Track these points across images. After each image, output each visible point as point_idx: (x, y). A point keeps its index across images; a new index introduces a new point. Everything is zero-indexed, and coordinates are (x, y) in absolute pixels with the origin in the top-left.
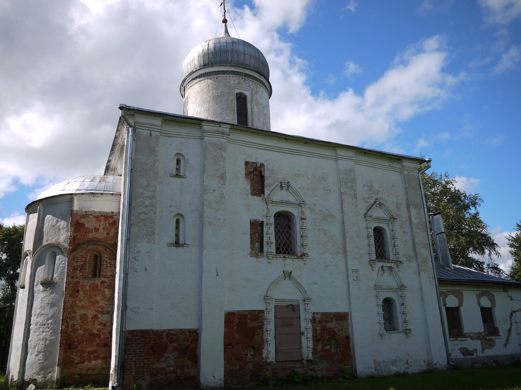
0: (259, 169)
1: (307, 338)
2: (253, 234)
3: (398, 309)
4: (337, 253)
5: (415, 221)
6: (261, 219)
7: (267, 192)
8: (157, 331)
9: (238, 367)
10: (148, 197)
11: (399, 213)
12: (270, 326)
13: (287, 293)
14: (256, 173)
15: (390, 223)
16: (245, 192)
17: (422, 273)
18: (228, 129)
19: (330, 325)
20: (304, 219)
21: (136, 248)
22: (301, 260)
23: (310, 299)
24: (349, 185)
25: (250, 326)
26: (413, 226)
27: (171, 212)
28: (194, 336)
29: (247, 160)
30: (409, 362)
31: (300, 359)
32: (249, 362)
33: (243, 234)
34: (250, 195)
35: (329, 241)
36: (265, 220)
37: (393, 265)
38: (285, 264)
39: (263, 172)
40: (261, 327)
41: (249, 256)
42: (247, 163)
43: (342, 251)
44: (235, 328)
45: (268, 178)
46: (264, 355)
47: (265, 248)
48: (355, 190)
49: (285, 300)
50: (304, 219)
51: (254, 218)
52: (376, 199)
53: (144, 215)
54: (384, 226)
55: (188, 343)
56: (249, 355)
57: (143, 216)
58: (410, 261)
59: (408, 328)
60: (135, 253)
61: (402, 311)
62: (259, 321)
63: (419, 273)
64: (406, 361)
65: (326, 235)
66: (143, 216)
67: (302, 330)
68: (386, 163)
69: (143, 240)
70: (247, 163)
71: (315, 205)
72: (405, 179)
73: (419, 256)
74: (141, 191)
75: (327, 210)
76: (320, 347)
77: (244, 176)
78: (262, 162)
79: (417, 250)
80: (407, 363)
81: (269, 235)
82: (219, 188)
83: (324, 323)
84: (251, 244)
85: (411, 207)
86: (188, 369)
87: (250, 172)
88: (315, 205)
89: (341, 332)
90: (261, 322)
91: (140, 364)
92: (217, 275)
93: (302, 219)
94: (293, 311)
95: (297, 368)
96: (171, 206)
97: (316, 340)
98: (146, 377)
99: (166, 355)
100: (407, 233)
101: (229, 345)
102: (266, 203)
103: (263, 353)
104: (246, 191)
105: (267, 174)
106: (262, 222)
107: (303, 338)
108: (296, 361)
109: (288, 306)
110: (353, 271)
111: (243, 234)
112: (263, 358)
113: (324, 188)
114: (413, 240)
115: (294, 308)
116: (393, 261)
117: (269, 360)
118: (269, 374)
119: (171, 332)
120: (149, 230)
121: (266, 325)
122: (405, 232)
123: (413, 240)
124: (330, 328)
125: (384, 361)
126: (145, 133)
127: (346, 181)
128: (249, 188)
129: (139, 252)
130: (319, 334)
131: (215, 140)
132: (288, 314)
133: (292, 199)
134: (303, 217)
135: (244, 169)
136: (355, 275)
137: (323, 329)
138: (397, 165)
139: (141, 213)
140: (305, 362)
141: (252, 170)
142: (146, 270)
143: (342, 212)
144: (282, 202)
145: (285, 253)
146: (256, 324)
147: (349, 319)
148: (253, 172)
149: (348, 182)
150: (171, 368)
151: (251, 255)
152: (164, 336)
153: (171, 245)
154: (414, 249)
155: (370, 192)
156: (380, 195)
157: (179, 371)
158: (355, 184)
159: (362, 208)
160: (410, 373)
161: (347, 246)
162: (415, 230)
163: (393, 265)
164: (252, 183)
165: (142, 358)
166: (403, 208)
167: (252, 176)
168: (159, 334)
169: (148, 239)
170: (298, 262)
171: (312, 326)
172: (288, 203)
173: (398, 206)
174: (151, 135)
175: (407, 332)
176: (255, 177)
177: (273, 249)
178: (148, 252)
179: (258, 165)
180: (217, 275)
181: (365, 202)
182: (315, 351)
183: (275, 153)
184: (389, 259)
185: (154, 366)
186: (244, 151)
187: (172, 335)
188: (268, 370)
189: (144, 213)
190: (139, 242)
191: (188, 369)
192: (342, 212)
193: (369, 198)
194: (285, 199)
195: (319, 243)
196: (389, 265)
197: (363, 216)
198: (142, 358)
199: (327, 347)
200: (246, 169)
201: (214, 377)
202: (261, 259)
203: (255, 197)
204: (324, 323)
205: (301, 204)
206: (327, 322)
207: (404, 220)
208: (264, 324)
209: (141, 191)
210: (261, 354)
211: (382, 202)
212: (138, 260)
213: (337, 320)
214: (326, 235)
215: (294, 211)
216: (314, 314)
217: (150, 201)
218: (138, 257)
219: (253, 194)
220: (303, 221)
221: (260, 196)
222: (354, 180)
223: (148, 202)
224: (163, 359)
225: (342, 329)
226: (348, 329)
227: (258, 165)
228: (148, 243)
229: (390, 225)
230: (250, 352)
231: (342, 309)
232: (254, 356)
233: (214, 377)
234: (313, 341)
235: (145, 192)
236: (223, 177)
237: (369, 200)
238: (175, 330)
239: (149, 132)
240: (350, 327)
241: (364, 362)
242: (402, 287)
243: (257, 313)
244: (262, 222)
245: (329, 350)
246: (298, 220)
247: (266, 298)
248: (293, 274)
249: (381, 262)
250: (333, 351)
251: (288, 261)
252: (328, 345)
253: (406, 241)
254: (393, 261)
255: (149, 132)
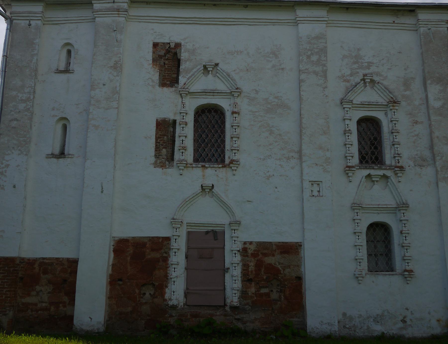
0: (173, 51)
1: (232, 276)
2: (159, 138)
3: (396, 239)
4: (288, 159)
5: (435, 104)
6: (171, 117)
7: (182, 80)
8: (29, 260)
9: (129, 309)
10: (22, 100)
11: (408, 93)
12: (178, 260)
13: (206, 214)
14: (168, 56)
15: (388, 109)
16: (151, 84)
17: (441, 184)
18: (126, 5)
19: (270, 260)
20: (238, 113)
21: (4, 162)
22: (228, 169)
23: (239, 223)
24: (314, 58)
25: (149, 257)
26: (431, 112)
27: (54, 116)
28: (72, 265)
29: (157, 41)
30: (407, 320)
31: (223, 304)
32: (146, 303)
33: (146, 138)
34: (157, 87)
35: (276, 142)
36: (178, 118)
37: (389, 173)
38: (204, 176)
39: (178, 55)
40: (166, 259)
41: (152, 166)
42: (155, 45)
43: (296, 156)
44: (129, 258)
45: (186, 61)
46: (167, 296)
47: (177, 156)
48: (324, 65)
49: (203, 225)
50: (238, 113)
51: (162, 116)
52: (365, 75)
53: (15, 122)
54: (380, 115)
55: (63, 275)
56: (147, 295)
57: (14, 124)
58: (421, 166)
59: (408, 268)
60: (3, 168)
61: (401, 242)
62: (163, 251)
63: (437, 183)
64: (401, 318)
65: (271, 133)
66: (14, 124)
67: (227, 265)
68: (389, 19)
69: (13, 151)
70: (155, 45)
71: (257, 92)
72: (421, 40)
73: (438, 158)
74: (14, 93)
75: (276, 98)
76: (253, 290)
77: (151, 62)
78: (178, 41)
79: (436, 148)
80: (404, 321)
81: (181, 138)
82: (111, 81)
83: (260, 256)
84: (156, 150)
85: (429, 82)
86: (65, 306)
87: (159, 56)
88: (257, 92)
89: (287, 270)
90: (166, 253)
91: (2, 297)
92: (102, 192)
93: (233, 113)
94: (216, 239)
95: (217, 315)
96: (53, 109)
97: (247, 278)
98: (7, 312)
99: (38, 288)
100: (422, 123)
101: (120, 280)
102: (181, 95)
103: (165, 293)
104: (153, 81)
105: (184, 55)
106: (175, 122)
107: (227, 276)
108: (217, 307)
109: (207, 233)
110: (313, 183)
111: (146, 138)
112: (166, 300)
113: (274, 66)
114: (431, 133)
115: (216, 235)
116: (391, 168)
117: (171, 303)
118: (172, 321)
119: (45, 261)
120: (21, 139)
121: (171, 257)
122: (416, 122)
123: (431, 133)
124: (270, 264)
125: (361, 315)
126: (23, 23)
127: (309, 53)
128: (156, 77)
129: (8, 166)
130: (252, 271)
131: (108, 20)
132: (206, 244)
133: (221, 86)
134: (236, 110)
135: (151, 54)
136: (316, 188)
137: (259, 264)
138: (408, 20)
139: (12, 120)
140: (227, 308)
141: (162, 53)
142: (14, 187)
143: (300, 99)
144: (205, 93)
145: (204, 161)
146: (157, 255)
147: (302, 252)
148: (165, 56)
149: (312, 54)
150: (44, 305)
151: (156, 165)
152: (36, 266)
153: (50, 156)
154: (432, 147)
155: (356, 66)
156: (373, 69)
157: (52, 308)
158: (326, 56)
159: (336, 89)
160: (407, 336)
161: (304, 147)
162: (433, 118)
163: (389, 173)
164: (161, 70)
165: (5, 290)
166: (417, 85)
167: (162, 61)
168: (30, 263)
169: (19, 150)
170: (222, 173)
171: (242, 260)
172: (213, 93)
173: (407, 84)
174: (30, 25)
175: (408, 274)
176: (167, 62)
177: (189, 156)
178: (18, 166)
179: (172, 45)
180: (102, 192)
181: (345, 81)
182: (244, 294)
183: (198, 26)
184: (385, 164)
185: (24, 300)
186: (153, 29)
187: (46, 265)
188: (171, 316)
189: (16, 120)
190: (9, 154)
191: (65, 306)
192: (300, 99)
193: (351, 75)
194: (211, 87)
195: (260, 146)
196: (381, 172)
197: (338, 102)
198: (5, 290)
199: (263, 291)
200: (154, 52)
201: (91, 319)
202: (169, 171)
203: (165, 89)
204: (260, 256)
205: (235, 92)
206: (265, 255)
207: (417, 103)
208: (169, 255)
209: (14, 93)
210: (163, 294)
211: (376, 78)
212: (5, 176)
213: (281, 253)
214: (271, 133)
215: (224, 103)
216: (245, 243)
217: (24, 105)
218: (6, 172)
219: (163, 84)
220: (235, 115)
221: (172, 87)
222: (323, 51)
223: (22, 106)
224: (34, 293)
225: (289, 267)
226: (299, 266)
227: (172, 45)
228: (19, 154)
229: (389, 112)
230: (149, 292)
231: (290, 237)
232: (153, 296)
233: (91, 319)
234: (243, 281)
235: (19, 94)
236: (117, 67)
237: (352, 78)
238: (50, 259)
239: (28, 22)
240: (303, 263)
241: (320, 313)
242: (402, 206)
243: (160, 240)
244: (175, 122)
245: (268, 295)
246: (228, 115)
247: (175, 222)
248: (215, 190)
249: (366, 168)
250: (274, 296)
251: (209, 171)
252: (266, 287)
253: (417, 135)
254: (391, 168)
255: (28, 22)
